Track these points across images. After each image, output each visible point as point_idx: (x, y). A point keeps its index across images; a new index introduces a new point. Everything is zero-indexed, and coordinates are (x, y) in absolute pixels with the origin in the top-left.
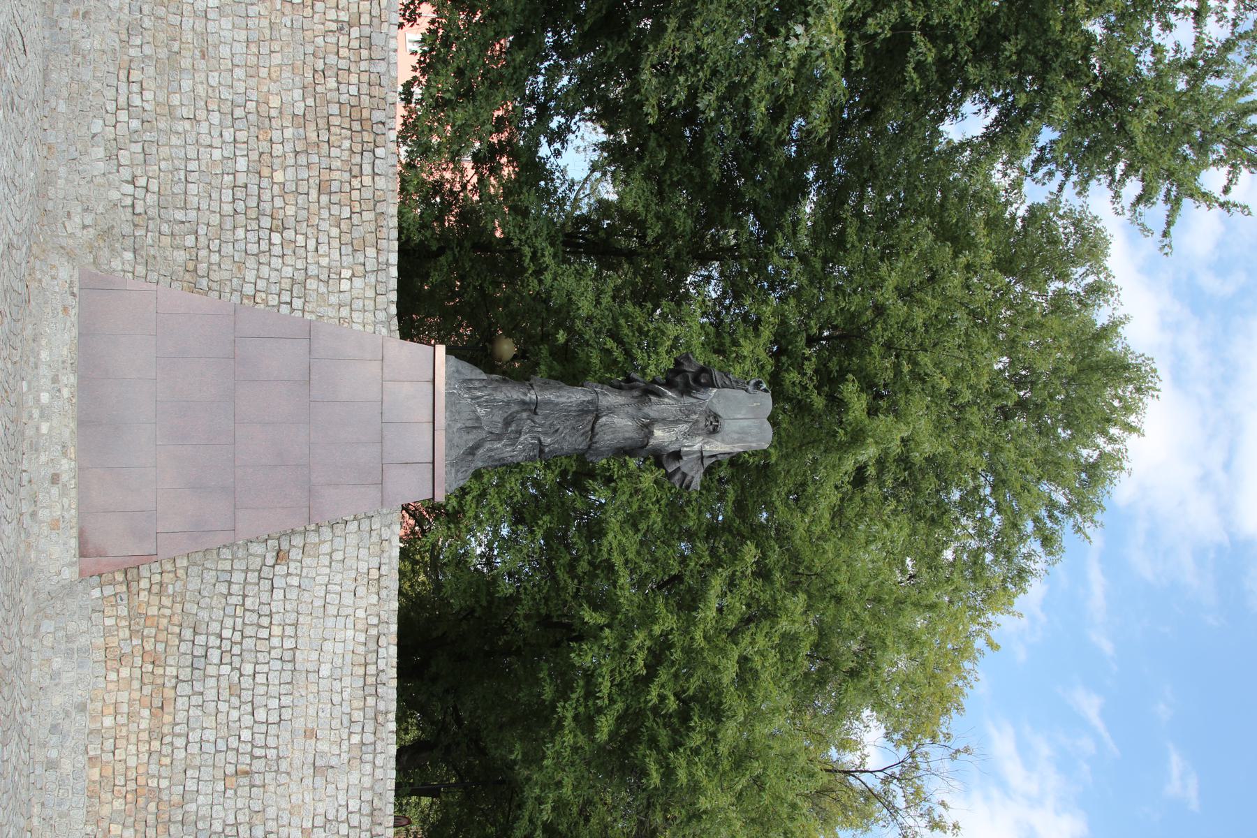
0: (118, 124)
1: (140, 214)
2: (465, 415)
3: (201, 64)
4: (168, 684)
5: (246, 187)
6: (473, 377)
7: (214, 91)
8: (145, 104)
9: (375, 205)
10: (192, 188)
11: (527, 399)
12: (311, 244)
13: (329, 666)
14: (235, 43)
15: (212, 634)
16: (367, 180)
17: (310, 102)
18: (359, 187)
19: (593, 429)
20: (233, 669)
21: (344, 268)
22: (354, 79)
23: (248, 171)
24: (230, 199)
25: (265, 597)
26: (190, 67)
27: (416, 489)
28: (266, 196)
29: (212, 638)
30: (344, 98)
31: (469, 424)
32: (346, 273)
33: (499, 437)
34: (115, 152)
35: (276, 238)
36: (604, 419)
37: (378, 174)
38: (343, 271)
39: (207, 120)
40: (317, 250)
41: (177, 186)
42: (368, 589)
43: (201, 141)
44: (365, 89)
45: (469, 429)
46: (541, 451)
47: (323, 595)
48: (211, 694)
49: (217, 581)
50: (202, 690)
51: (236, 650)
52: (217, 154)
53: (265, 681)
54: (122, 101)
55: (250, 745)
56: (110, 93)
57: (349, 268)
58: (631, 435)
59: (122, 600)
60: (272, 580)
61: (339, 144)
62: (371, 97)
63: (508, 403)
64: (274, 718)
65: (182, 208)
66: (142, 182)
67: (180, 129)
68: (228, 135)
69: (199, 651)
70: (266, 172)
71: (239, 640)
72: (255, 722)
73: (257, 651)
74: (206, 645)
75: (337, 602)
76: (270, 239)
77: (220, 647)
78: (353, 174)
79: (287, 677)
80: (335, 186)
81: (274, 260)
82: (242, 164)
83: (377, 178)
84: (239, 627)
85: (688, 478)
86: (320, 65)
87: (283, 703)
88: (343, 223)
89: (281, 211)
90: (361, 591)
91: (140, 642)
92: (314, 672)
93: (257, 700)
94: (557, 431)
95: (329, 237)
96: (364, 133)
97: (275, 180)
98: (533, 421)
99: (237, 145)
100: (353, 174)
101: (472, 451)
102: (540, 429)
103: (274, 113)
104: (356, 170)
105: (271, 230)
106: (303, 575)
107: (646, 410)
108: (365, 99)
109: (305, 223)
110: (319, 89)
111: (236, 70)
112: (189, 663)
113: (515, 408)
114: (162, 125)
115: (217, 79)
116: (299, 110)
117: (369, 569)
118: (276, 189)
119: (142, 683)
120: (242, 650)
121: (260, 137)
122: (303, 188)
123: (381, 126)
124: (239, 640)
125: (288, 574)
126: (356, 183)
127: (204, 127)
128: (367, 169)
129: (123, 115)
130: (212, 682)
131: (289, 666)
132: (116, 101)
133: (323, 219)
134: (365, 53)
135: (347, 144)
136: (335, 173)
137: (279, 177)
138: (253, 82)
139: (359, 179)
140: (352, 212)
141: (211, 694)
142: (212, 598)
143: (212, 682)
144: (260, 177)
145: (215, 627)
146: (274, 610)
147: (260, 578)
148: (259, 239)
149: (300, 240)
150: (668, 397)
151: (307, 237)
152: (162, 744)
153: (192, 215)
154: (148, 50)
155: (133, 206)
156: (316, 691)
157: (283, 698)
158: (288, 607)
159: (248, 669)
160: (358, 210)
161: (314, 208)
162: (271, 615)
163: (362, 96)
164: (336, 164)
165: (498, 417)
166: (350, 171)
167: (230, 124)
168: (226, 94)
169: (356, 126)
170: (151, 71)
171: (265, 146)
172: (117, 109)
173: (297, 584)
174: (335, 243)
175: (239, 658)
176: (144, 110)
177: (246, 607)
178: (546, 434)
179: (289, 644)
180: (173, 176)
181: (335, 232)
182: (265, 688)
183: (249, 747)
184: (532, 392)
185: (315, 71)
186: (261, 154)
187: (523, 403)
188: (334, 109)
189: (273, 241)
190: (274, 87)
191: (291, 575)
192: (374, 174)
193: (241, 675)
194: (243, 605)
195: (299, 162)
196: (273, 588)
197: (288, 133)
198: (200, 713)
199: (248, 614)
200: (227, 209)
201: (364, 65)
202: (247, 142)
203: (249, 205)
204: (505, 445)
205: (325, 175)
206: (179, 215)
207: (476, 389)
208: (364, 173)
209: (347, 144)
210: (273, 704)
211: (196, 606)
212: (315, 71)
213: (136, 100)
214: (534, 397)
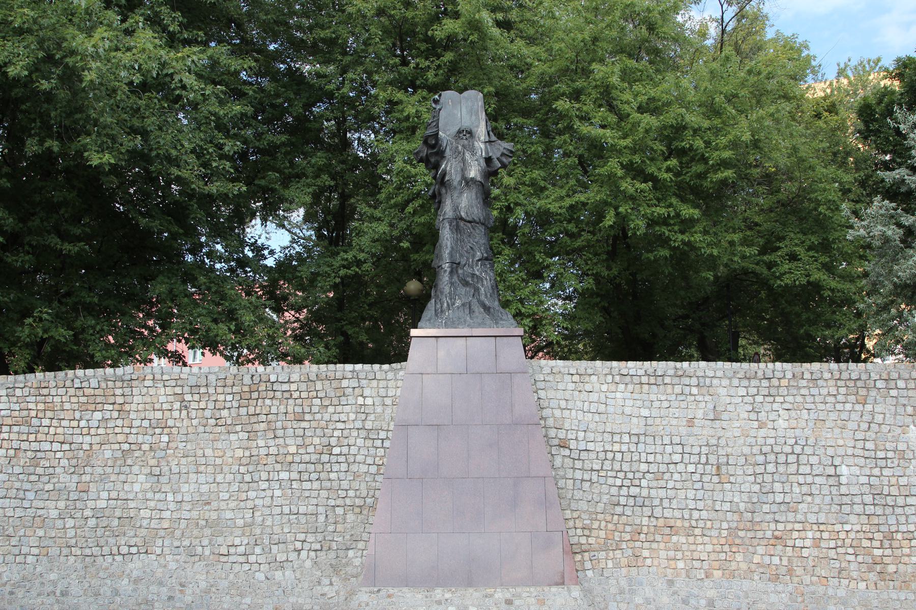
2: (461, 314)
3: (214, 505)
5: (300, 472)
6: (433, 308)
7: (233, 496)
9: (311, 381)
10: (302, 510)
11: (449, 270)
12: (340, 425)
14: (199, 482)
16: (294, 387)
19: (470, 222)
21: (356, 403)
22: (221, 398)
25: (593, 456)
26: (216, 513)
27: (514, 350)
28: (306, 458)
29: (622, 493)
30: (235, 404)
31: (467, 311)
32: (360, 400)
33: (477, 290)
34: (278, 564)
35: (336, 450)
36: (463, 214)
39: (253, 500)
40: (344, 422)
43: (268, 504)
44: (228, 390)
45: (471, 311)
46: (486, 259)
48: (662, 493)
50: (659, 500)
51: (630, 475)
53: (653, 455)
55: (698, 466)
57: (356, 399)
58: (474, 194)
59: (595, 556)
60: (580, 451)
63: (452, 284)
67: (261, 519)
69: (631, 501)
71: (623, 474)
73: (631, 461)
75: (596, 404)
77: (628, 487)
78: (289, 397)
79: (650, 440)
81: (352, 452)
82: (284, 475)
83: (292, 380)
84: (614, 474)
85: (505, 152)
86: (212, 422)
87: (669, 442)
88: (324, 404)
90: (588, 387)
94: (471, 248)
96: (260, 389)
97: (295, 452)
100: (289, 397)
101: (487, 309)
102: (471, 260)
104: (287, 395)
107: (455, 183)
112: (639, 509)
113: (455, 278)
118: (301, 451)
119: (654, 541)
120: (631, 471)
123: (254, 378)
124: (623, 474)
125: (576, 439)
126: (296, 395)
128: (285, 387)
130: (653, 493)
131: (642, 438)
134: (203, 390)
135: (268, 402)
136: (289, 410)
137: (293, 449)
139: (293, 393)
140: (317, 397)
141: (662, 493)
143: (653, 493)
144: (293, 462)
145: (614, 491)
147: (579, 459)
148: (337, 462)
149: (337, 433)
152: (697, 527)
153: (321, 509)
154: (205, 542)
155: (316, 551)
156: (660, 419)
158: (600, 439)
160: (315, 393)
161: (314, 424)
162: (606, 451)
163: (234, 391)
165: (462, 290)
166: (287, 399)
168: (235, 487)
170: (220, 540)
171: (271, 459)
174: (339, 409)
175: (636, 473)
176: (248, 544)
178: (474, 256)
179: (626, 438)
180: (294, 523)
181: (331, 409)
182: (658, 455)
184: (443, 266)
185: (216, 425)
187: (451, 272)
189: (339, 453)
190: (229, 454)
191: (577, 437)
193: (648, 472)
196: (586, 450)
198: (675, 500)
200: (316, 485)
204: (483, 285)
206: (322, 518)
207: (442, 307)
208: (288, 389)
210: (669, 449)
212: (216, 425)
213: (241, 549)
214: (447, 265)
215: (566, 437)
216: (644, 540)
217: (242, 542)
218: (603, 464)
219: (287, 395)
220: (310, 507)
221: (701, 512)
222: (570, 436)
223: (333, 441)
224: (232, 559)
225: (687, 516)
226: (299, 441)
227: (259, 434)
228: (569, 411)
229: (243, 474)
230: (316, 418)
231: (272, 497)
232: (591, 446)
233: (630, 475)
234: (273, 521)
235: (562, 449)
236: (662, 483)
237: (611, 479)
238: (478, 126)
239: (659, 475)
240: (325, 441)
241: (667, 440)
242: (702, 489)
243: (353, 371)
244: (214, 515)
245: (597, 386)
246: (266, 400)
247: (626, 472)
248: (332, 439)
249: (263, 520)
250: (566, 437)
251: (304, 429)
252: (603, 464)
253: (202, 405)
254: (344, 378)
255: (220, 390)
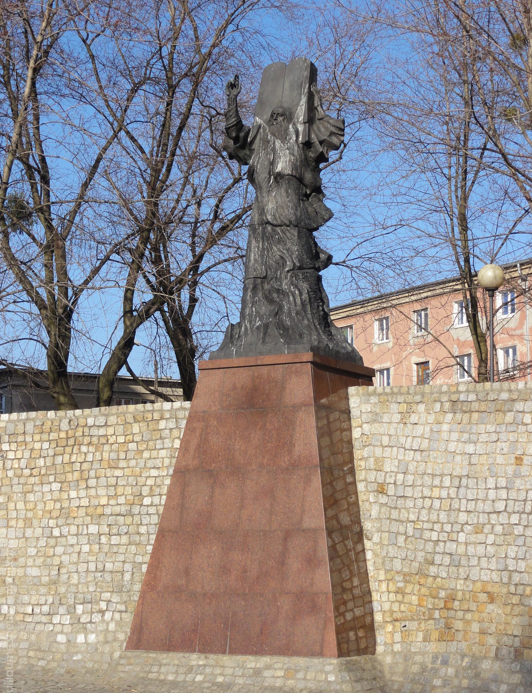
0: (62, 622)
1: (126, 607)
3: (22, 560)
4: (471, 588)
5: (110, 525)
7: (40, 551)
8: (48, 603)
9: (128, 423)
10: (109, 566)
12: (154, 472)
13: (466, 446)
14: (8, 536)
15: (435, 549)
16: (110, 431)
17: (52, 478)
18: (114, 437)
20: (462, 531)
21: (173, 446)
22: (37, 446)
23: (99, 524)
24: (118, 537)
25: (410, 503)
26: (23, 569)
28: (117, 509)
29: (438, 549)
30: (51, 452)
34: (81, 626)
35: (147, 501)
36: (269, 218)
37: (106, 422)
38: (175, 447)
39: (60, 556)
40: (158, 468)
41: (106, 579)
42: (413, 412)
43: (75, 560)
44: (45, 437)
47: (412, 452)
48: (480, 550)
49: (396, 545)
50: (476, 558)
51: (448, 528)
52: (86, 548)
53: (474, 502)
54: (44, 619)
55: (522, 515)
56: (39, 627)
57: (173, 441)
59: (405, 626)
60: (397, 497)
61: (83, 455)
62: (51, 431)
64: (503, 494)
65: (122, 575)
66: (103, 605)
67: (66, 576)
68: (72, 540)
69: (447, 560)
70: (99, 510)
71: (440, 525)
72: (505, 510)
73: (450, 510)
74: (443, 553)
75: (419, 439)
76: (148, 506)
77: (444, 541)
78: (105, 442)
79: (472, 482)
80: (113, 455)
82: (93, 529)
83: (109, 424)
84: (430, 526)
85: (333, 129)
86: (27, 472)
87: (493, 486)
88: (140, 448)
89: (128, 497)
91: (437, 611)
92: (470, 458)
93: (488, 509)
95: (150, 458)
96: (76, 435)
97: (106, 503)
98: (272, 279)
99: (80, 533)
100: (105, 442)
103: (58, 505)
104: (103, 440)
105: (141, 505)
106: (396, 470)
108: (53, 436)
109: (139, 478)
110: (43, 472)
111: (27, 535)
112: (455, 569)
114: (62, 590)
115: (32, 549)
116: (56, 486)
117: (399, 413)
118: (112, 502)
119: (468, 610)
120: (448, 523)
121: (75, 515)
122: (113, 481)
123: (72, 423)
124: (440, 525)
125: (395, 483)
126: (112, 440)
127: (65, 559)
128: (102, 432)
129: (56, 619)
130: (471, 550)
131: (464, 481)
132: (45, 624)
133: (137, 464)
134: (20, 438)
135: (84, 449)
136: (104, 457)
137: (104, 501)
138: (35, 522)
139: (109, 437)
140: (133, 441)
141: (480, 550)
142: (408, 549)
143: (471, 550)
144: (103, 514)
145: (430, 547)
146: (420, 495)
147: (396, 508)
148: (147, 514)
149: (150, 482)
150: (253, 163)
151: (149, 477)
152: (515, 594)
153: (128, 567)
154: (11, 600)
155: (121, 612)
156: (485, 456)
157: (489, 486)
158: (419, 482)
159: (463, 517)
160: (131, 437)
161: (127, 472)
162: (424, 498)
163: (51, 438)
164: (98, 457)
166: (104, 444)
167: (64, 539)
168: (42, 543)
169: (71, 442)
170: (26, 598)
171: (82, 512)
172: (51, 623)
173: (403, 475)
174: (154, 453)
175: (454, 526)
176: (53, 603)
177: (416, 520)
179: (447, 481)
180: (99, 581)
181: (146, 455)
182: (480, 501)
183: (524, 516)
185: (31, 475)
186: (87, 515)
188: (59, 459)
189: (149, 503)
190: (40, 506)
192: (106, 425)
193: (467, 523)
194: (413, 522)
195: (94, 485)
196: (403, 496)
197: (73, 494)
198: (494, 559)
199: (421, 518)
200: (124, 539)
201: (29, 439)
202: (78, 526)
203: (123, 523)
205: (105, 464)
206: (127, 576)
208: (105, 433)
209: (84, 449)
210: (492, 494)
211: (414, 563)
212: (31, 475)
213: (45, 609)
215: (385, 480)
216: (458, 608)
217: (46, 601)
218: (419, 513)
219: (103, 440)
220: (116, 563)
221: (522, 574)
222: (388, 481)
223: (145, 491)
224: (37, 618)
225: (505, 580)
226: (112, 492)
227: (72, 484)
228: (390, 449)
229: (52, 528)
230: (131, 465)
231: (79, 553)
232: (409, 492)
233: (448, 528)
234: (79, 578)
235: (380, 495)
236: (481, 537)
237: (427, 532)
238: (298, 104)
239: (479, 529)
240: (136, 490)
241: (491, 482)
242: (524, 545)
243: (9, 421)
244: (20, 572)
245: (424, 416)
246: (82, 446)
247: (443, 524)
248: (144, 488)
249: (69, 577)
250: (385, 480)
251: (118, 477)
252: (419, 513)
253: (19, 455)
254: (162, 418)
255: (37, 437)
